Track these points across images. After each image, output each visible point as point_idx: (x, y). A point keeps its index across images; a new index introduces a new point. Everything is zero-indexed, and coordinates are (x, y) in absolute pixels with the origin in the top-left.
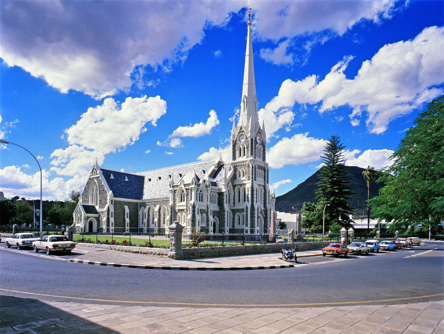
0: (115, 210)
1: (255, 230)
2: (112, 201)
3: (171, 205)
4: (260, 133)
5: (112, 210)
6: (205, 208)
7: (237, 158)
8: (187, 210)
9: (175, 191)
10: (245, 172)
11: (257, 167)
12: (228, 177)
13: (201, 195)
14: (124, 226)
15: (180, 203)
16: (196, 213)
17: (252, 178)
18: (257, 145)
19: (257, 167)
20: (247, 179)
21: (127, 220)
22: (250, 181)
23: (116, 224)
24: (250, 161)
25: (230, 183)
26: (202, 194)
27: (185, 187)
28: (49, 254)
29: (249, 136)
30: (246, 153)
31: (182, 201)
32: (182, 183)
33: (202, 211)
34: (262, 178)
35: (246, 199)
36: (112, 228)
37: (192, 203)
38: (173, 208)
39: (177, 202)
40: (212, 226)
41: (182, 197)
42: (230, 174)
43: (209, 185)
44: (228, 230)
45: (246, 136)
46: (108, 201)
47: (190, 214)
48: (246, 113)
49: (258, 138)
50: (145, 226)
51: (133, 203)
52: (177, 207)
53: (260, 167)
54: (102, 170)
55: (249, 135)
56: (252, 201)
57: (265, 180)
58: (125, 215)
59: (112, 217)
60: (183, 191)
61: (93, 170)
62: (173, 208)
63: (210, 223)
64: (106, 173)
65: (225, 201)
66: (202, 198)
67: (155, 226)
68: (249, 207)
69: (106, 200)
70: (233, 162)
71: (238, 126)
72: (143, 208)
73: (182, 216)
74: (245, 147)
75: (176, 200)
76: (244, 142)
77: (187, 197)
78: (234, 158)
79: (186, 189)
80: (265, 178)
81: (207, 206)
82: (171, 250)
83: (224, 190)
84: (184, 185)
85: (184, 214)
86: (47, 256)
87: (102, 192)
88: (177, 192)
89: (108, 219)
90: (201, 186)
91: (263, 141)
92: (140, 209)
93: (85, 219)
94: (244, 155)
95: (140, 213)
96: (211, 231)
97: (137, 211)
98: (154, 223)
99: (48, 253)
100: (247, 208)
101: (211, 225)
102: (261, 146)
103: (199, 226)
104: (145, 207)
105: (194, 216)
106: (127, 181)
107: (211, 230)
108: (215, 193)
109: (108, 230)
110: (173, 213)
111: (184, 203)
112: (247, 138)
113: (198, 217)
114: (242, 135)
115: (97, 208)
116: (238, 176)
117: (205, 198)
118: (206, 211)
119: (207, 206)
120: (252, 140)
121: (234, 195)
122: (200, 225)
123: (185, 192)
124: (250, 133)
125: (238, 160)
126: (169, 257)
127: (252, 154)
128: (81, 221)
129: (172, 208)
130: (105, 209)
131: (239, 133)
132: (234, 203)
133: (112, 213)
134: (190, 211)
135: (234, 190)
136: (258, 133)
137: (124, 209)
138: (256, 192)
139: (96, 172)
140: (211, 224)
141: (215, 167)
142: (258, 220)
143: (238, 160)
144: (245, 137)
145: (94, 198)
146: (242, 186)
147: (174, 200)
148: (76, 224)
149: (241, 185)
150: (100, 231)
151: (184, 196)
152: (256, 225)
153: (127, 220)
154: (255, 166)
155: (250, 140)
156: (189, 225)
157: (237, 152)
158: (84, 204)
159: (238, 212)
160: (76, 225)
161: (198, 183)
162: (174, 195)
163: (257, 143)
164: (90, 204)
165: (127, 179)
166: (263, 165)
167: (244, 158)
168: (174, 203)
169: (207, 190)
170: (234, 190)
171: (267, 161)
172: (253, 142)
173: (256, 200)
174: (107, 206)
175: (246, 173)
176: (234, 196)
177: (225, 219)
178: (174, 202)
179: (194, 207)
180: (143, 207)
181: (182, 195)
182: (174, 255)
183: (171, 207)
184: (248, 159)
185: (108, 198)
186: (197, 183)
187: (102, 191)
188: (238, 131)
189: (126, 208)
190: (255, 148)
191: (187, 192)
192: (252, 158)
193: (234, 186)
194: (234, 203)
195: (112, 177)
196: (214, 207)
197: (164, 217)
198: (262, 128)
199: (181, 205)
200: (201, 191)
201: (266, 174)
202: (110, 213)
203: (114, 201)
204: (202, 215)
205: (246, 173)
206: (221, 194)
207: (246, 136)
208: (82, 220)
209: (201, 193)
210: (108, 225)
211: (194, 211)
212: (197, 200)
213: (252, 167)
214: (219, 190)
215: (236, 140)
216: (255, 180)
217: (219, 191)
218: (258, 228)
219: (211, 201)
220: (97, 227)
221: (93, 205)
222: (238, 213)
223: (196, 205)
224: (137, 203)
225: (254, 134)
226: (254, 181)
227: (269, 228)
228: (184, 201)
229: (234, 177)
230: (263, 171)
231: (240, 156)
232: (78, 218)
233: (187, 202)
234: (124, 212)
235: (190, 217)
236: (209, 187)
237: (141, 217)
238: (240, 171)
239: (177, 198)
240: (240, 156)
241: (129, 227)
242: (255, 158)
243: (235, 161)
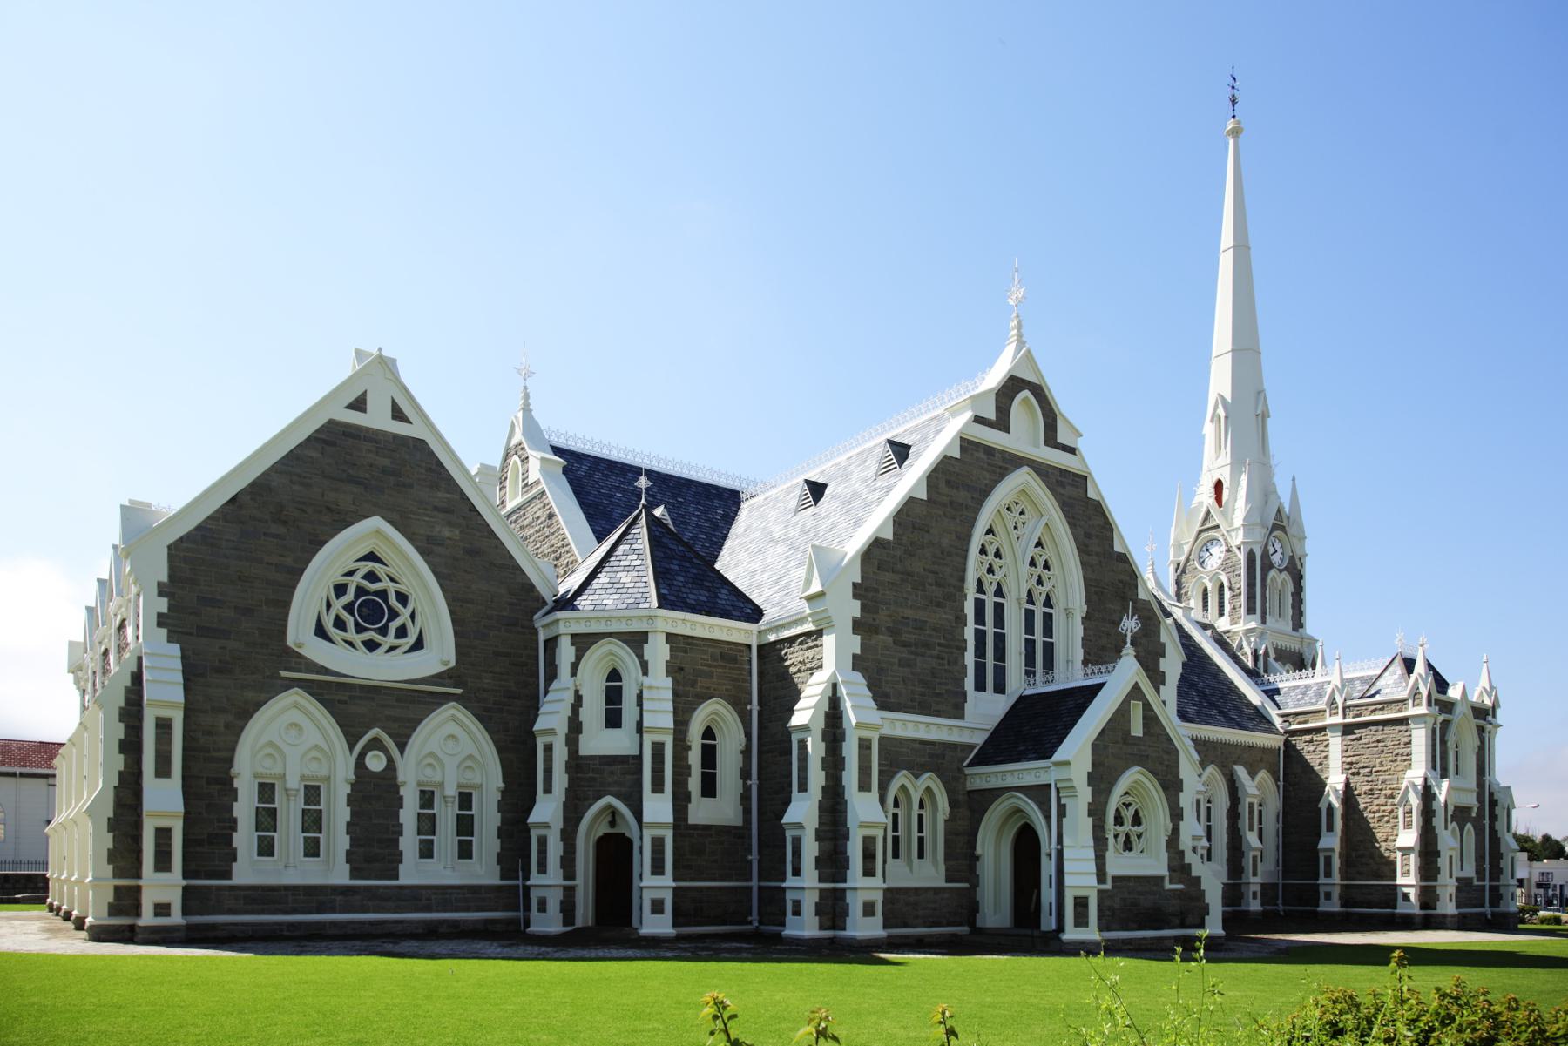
4: (1283, 529)
18: (1272, 573)
19: (1272, 655)
24: (1248, 632)
29: (1238, 542)
33: (1460, 815)
36: (1447, 887)
37: (1419, 782)
55: (1237, 539)
74: (1222, 586)
90: (1459, 710)
91: (1292, 558)
96: (1255, 894)
102: (1285, 575)
107: (1253, 888)
109: (1428, 896)
113: (1447, 840)
114: (1212, 540)
122: (1457, 873)
124: (1241, 533)
127: (1251, 610)
136: (1275, 527)
150: (1373, 904)
155: (1242, 557)
161: (1441, 697)
163: (1271, 566)
171: (1311, 626)
172: (1257, 566)
179: (1427, 795)
186: (1435, 695)
188: (1197, 527)
192: (1252, 625)
198: (1287, 510)
211: (1427, 812)
212: (1434, 768)
215: (1188, 560)
225: (1259, 535)
242: (1264, 621)
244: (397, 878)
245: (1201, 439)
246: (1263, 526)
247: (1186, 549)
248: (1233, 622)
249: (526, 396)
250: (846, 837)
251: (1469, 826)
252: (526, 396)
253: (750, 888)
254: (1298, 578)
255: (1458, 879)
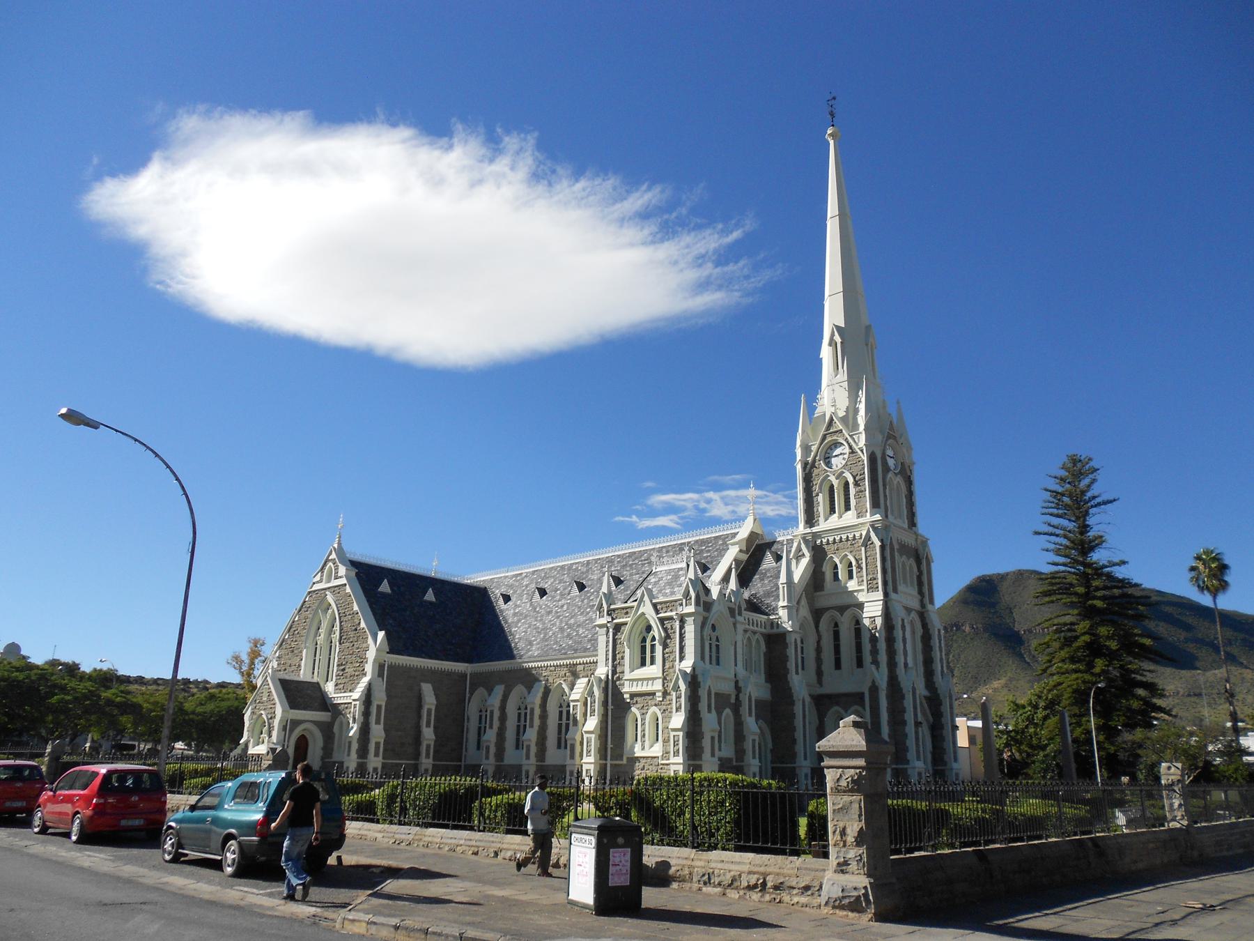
0: (389, 696)
1: (910, 772)
2: (381, 667)
3: (603, 677)
4: (895, 438)
5: (380, 698)
6: (728, 688)
7: (821, 519)
8: (665, 693)
9: (618, 628)
10: (854, 563)
11: (896, 547)
12: (796, 578)
13: (714, 643)
14: (417, 755)
15: (637, 672)
16: (703, 706)
17: (885, 583)
18: (890, 475)
20: (865, 587)
21: (428, 734)
22: (879, 595)
23: (391, 748)
25: (804, 602)
26: (717, 640)
27: (657, 612)
28: (78, 842)
30: (853, 502)
31: (643, 664)
32: (646, 598)
33: (721, 701)
34: (912, 585)
35: (867, 658)
38: (611, 690)
39: (627, 669)
40: (754, 757)
41: (643, 649)
42: (800, 570)
43: (740, 607)
44: (809, 771)
45: (851, 447)
46: (369, 668)
47: (678, 710)
48: (843, 376)
49: (890, 452)
50: (487, 758)
51: (449, 674)
52: (627, 683)
53: (904, 549)
54: (354, 564)
56: (892, 664)
57: (921, 593)
58: (420, 717)
59: (378, 722)
60: (649, 628)
61: (325, 564)
62: (611, 690)
63: (748, 745)
64: (368, 576)
65: (791, 665)
66: (718, 652)
67: (528, 757)
68: (883, 683)
69: (363, 661)
70: (808, 530)
71: (818, 413)
72: (486, 693)
73: (648, 717)
75: (623, 658)
76: (846, 465)
77: (665, 646)
78: (810, 520)
79: (662, 620)
80: (920, 584)
81: (737, 682)
82: (842, 867)
83: (788, 626)
84: (655, 606)
85: (654, 709)
86: (70, 850)
87: (351, 637)
88: (626, 629)
89: (365, 730)
90: (715, 609)
92: (471, 694)
93: (284, 728)
94: (848, 508)
95: (472, 710)
96: (806, 775)
97: (461, 702)
98: (484, 745)
99: (74, 838)
100: (874, 689)
101: (754, 752)
103: (713, 755)
104: (490, 691)
105: (694, 719)
106: (431, 603)
108: (757, 636)
110: (610, 707)
111: (654, 670)
112: (853, 452)
113: (709, 721)
114: (837, 444)
115: (329, 688)
116: (829, 576)
117: (727, 653)
118: (733, 701)
119: (737, 682)
120: (872, 459)
121: (818, 642)
123: (657, 631)
125: (822, 526)
126: (838, 904)
127: (875, 504)
128: (270, 736)
129: (606, 690)
130: (357, 693)
131: (824, 437)
132: (819, 673)
133: (379, 707)
134: (679, 697)
135: (817, 627)
136: (890, 437)
137: (420, 698)
138: (901, 633)
139: (337, 569)
140: (754, 746)
141: (741, 551)
142: (917, 733)
143: (822, 526)
144: (847, 450)
145: (322, 657)
146: (848, 613)
147: (614, 659)
148: (250, 745)
149: (842, 609)
151: (653, 647)
152: (911, 755)
153: (428, 734)
154: (891, 543)
156: (676, 753)
157: (821, 500)
158: (287, 678)
159: (837, 704)
160: (251, 751)
161: (707, 599)
162: (614, 640)
164: (304, 675)
165: (430, 596)
166: (909, 540)
167: (850, 518)
168: (614, 672)
169: (734, 624)
170: (817, 627)
171: (923, 527)
173: (903, 660)
174: (365, 681)
175: (859, 567)
176: (819, 650)
177: (794, 729)
178: (614, 667)
180: (481, 691)
181: (644, 640)
182: (866, 895)
183: (603, 685)
184: (861, 520)
185: (371, 654)
187: (352, 634)
189: (427, 689)
190: (884, 485)
191: (665, 630)
192: (878, 517)
193: (817, 614)
194: (819, 673)
195: (385, 587)
196: (757, 688)
197: (560, 725)
198: (895, 421)
199: (641, 678)
200: (714, 627)
201: (925, 572)
202: (374, 710)
203: (391, 667)
204: (719, 714)
205: (859, 567)
206: (775, 639)
207: (851, 447)
208: (275, 734)
209: (714, 635)
210: (363, 752)
211: (693, 699)
212: (703, 658)
213: (883, 548)
214: (768, 627)
215: (814, 461)
216: (895, 590)
217: (768, 631)
218: (919, 765)
219: (747, 666)
220: (322, 758)
221: (315, 679)
222: (836, 708)
223: (700, 679)
224: (463, 676)
226: (893, 596)
227: (955, 765)
228: (652, 663)
229: (817, 579)
230: (912, 562)
231: (832, 511)
232: (260, 722)
233: (664, 665)
234: (420, 707)
235: (678, 720)
236: (740, 614)
237: (472, 725)
238: (837, 560)
239: (627, 651)
240: (832, 511)
241: (431, 760)
243: (815, 529)
244: (863, 694)
245: (818, 363)
246: (881, 432)
247: (814, 448)
248: (860, 515)
249: (94, 425)
250: (903, 697)
251: (727, 711)
252: (94, 425)
253: (474, 675)
254: (909, 482)
255: (720, 759)
